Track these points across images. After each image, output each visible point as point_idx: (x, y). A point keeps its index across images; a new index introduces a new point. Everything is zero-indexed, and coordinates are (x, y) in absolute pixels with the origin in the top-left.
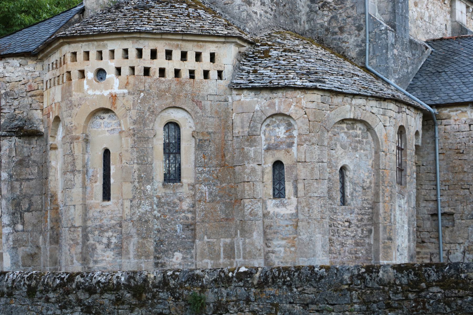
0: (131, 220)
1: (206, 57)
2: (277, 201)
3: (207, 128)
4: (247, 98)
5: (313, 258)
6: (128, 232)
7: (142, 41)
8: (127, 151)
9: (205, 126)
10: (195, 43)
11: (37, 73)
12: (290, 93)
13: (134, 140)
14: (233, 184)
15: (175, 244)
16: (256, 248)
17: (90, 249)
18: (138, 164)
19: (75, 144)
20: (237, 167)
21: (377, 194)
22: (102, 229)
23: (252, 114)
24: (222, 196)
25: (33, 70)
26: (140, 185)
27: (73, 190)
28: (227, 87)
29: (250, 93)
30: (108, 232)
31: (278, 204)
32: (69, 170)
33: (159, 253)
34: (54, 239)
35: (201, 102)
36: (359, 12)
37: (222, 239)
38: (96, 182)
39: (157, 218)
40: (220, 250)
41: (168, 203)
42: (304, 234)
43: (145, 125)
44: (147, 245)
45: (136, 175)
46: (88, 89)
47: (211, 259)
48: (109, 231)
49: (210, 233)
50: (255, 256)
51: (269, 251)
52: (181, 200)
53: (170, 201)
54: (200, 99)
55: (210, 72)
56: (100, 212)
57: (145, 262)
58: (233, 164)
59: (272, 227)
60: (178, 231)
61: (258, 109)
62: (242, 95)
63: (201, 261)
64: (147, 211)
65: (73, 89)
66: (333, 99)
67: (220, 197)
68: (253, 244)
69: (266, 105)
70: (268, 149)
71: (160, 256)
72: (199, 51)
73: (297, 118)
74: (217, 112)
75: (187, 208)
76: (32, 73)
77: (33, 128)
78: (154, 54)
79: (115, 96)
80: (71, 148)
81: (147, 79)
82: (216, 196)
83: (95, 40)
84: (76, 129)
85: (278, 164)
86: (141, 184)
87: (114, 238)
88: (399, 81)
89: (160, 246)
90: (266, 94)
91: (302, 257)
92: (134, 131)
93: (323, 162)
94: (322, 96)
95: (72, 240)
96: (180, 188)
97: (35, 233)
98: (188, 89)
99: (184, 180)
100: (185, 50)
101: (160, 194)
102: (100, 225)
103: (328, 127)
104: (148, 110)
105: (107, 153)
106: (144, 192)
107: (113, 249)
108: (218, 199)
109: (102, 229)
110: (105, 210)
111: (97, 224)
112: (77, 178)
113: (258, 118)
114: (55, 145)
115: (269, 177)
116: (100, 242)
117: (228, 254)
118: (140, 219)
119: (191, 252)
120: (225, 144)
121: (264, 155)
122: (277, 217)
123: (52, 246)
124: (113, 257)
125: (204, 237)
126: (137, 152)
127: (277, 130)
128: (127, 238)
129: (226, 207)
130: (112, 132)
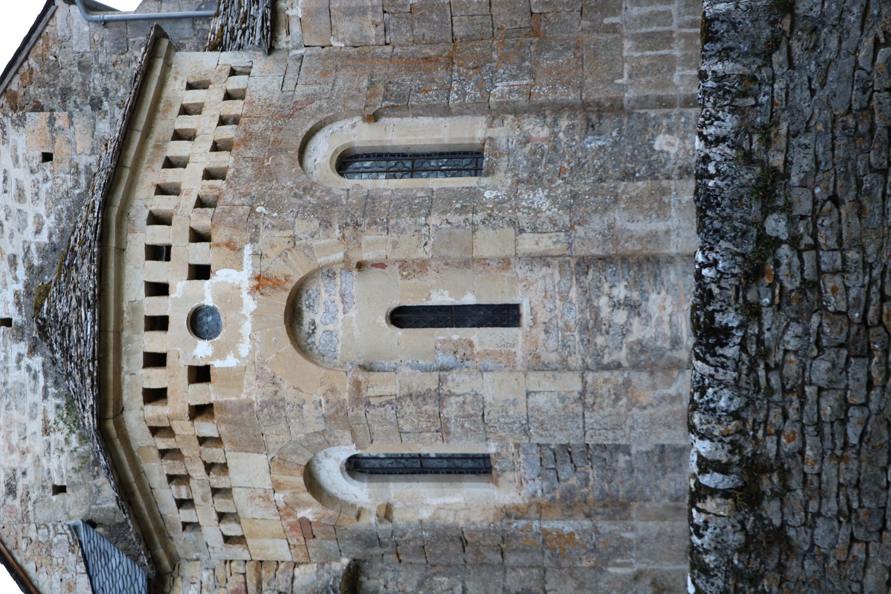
0: (568, 230)
6: (600, 237)
7: (133, 212)
8: (395, 244)
11: (206, 575)
13: (369, 225)
17: (643, 357)
18: (427, 216)
19: (371, 392)
20: (456, 29)
22: (590, 326)
25: (198, 586)
26: (482, 210)
27: (489, 399)
28: (271, 57)
30: (598, 308)
32: (437, 409)
34: (616, 512)
35: (296, 102)
36: (190, 34)
37: (625, 54)
38: (471, 344)
41: (533, 165)
43: (335, 202)
45: (455, 219)
46: (237, 356)
47: (672, 70)
48: (595, 304)
52: (527, 140)
53: (528, 160)
54: (289, 103)
56: (546, 332)
60: (600, 143)
62: (290, 12)
64: (547, 196)
65: (233, 399)
67: (523, 60)
72: (177, 109)
74: (324, 74)
76: (204, 589)
77: (338, 585)
79: (258, 278)
80: (382, 405)
82: (520, 68)
83: (118, 333)
84: (333, 390)
87: (615, 292)
92: (347, 224)
95: (618, 398)
96: (497, 142)
97: (601, 584)
98: (262, 126)
100: (171, 134)
101: (509, 181)
102: (580, 332)
104: (301, 198)
105: (401, 317)
106: (499, 203)
107: (643, 293)
109: (592, 326)
110: (543, 316)
111: (578, 339)
112: (458, 385)
114: (379, 507)
116: (625, 332)
119: (654, 118)
120: (401, 57)
123: (634, 515)
124: (663, 293)
125: (618, 84)
128: (616, 241)
130: (347, 299)
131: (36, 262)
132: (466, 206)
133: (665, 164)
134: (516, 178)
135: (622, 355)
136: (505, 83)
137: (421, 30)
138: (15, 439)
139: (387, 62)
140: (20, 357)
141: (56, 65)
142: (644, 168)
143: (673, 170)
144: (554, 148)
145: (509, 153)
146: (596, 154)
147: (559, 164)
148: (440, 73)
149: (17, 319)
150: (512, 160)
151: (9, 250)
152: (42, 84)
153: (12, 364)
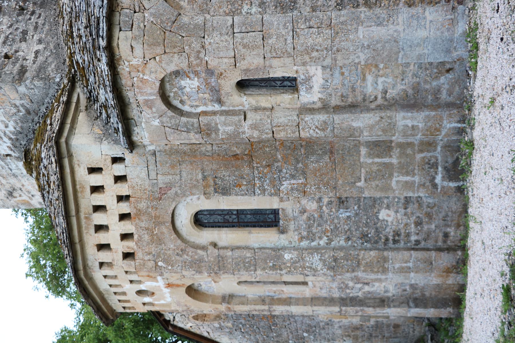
1: (95, 180)
2: (302, 89)
3: (198, 181)
4: (142, 134)
5: (401, 43)
7: (90, 263)
9: (195, 183)
10: (79, 195)
12: (125, 81)
14: (277, 143)
15: (367, 219)
16: (377, 123)
18: (255, 270)
23: (167, 129)
24: (297, 159)
26: (285, 268)
29: (136, 132)
31: (306, 88)
33: (380, 238)
35: (160, 188)
37: (362, 160)
39: (330, 240)
40: (378, 163)
41: (309, 228)
42: (358, 57)
44: (368, 260)
47: (391, 176)
49: (352, 177)
50: (390, 123)
51: (382, 98)
52: (303, 211)
53: (306, 224)
54: (156, 189)
55: (116, 175)
57: (392, 263)
58: (246, 143)
59: (345, 94)
60: (348, 214)
61: (158, 120)
63: (394, 191)
64: (320, 259)
66: (125, 6)
67: (298, 162)
68: (371, 127)
69: (149, 111)
70: (220, 101)
71: (383, 237)
72: (88, 190)
73: (163, 71)
74: (173, 167)
75: (315, 203)
78: (103, 247)
79: (168, 284)
81: (139, 255)
82: (296, 169)
85: (243, 85)
86: (283, 266)
89: (369, 238)
90: (133, 112)
91: (397, 59)
93: (233, 25)
94: (120, 30)
96: (287, 211)
99: (275, 206)
101: (297, 237)
103: (173, 14)
104: (181, 256)
106: (294, 263)
108: (300, 165)
113: (173, 121)
117: (385, 150)
118: (331, 268)
121: (229, 106)
122: (328, 88)
125: (359, 187)
126: (239, 271)
127: (188, 89)
129: (313, 154)
132: (275, 265)
133: (385, 229)
134: (300, 236)
136: (288, 182)
139: (211, 159)
142: (373, 231)
143: (390, 232)
144: (321, 216)
145: (295, 218)
146: (346, 221)
147: (324, 227)
150: (296, 223)
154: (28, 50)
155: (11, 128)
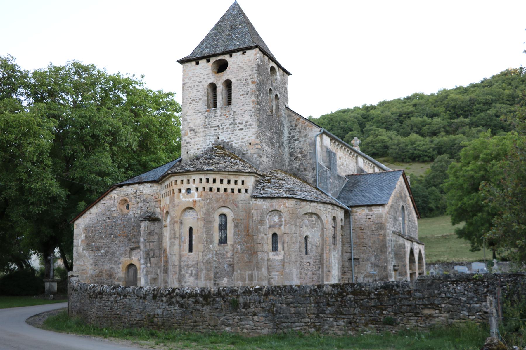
1: (239, 182)
2: (274, 253)
4: (259, 202)
7: (208, 175)
12: (280, 200)
21: (323, 249)
39: (215, 261)
45: (205, 240)
47: (242, 281)
52: (227, 252)
68: (262, 274)
70: (270, 227)
72: (236, 179)
74: (245, 209)
81: (211, 193)
85: (275, 235)
88: (333, 194)
90: (269, 200)
99: (228, 242)
105: (191, 229)
109: (188, 267)
110: (190, 257)
115: (270, 241)
116: (187, 273)
118: (207, 261)
131: (229, 144)
135: (183, 272)
137: (254, 228)
138: (197, 143)
140: (211, 142)
141: (306, 129)
145: (224, 249)
148: (244, 234)
149: (219, 140)
151: (232, 138)
152: (302, 126)
153: (210, 140)
154: (264, 159)
155: (234, 145)
